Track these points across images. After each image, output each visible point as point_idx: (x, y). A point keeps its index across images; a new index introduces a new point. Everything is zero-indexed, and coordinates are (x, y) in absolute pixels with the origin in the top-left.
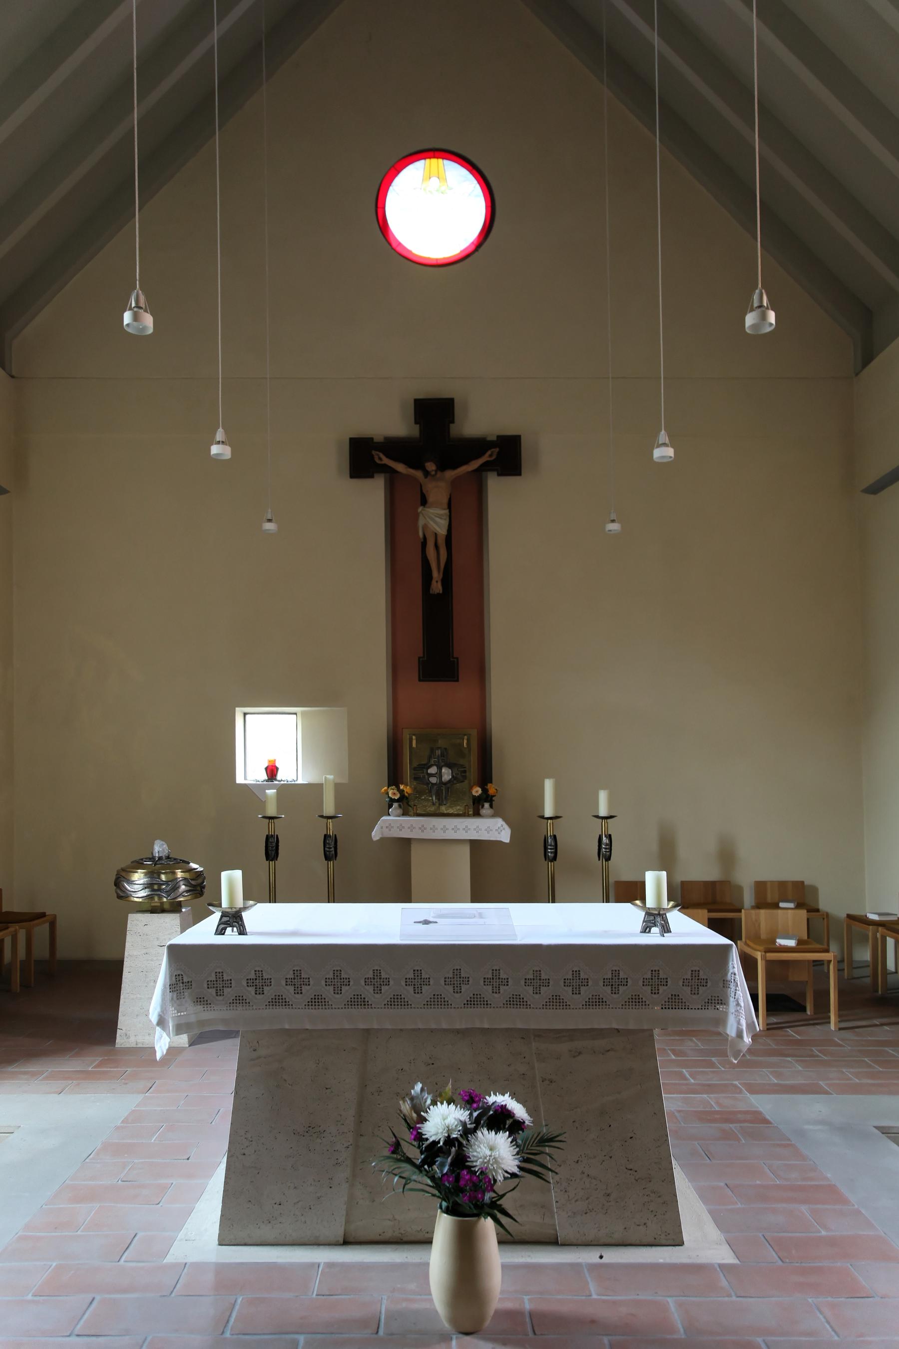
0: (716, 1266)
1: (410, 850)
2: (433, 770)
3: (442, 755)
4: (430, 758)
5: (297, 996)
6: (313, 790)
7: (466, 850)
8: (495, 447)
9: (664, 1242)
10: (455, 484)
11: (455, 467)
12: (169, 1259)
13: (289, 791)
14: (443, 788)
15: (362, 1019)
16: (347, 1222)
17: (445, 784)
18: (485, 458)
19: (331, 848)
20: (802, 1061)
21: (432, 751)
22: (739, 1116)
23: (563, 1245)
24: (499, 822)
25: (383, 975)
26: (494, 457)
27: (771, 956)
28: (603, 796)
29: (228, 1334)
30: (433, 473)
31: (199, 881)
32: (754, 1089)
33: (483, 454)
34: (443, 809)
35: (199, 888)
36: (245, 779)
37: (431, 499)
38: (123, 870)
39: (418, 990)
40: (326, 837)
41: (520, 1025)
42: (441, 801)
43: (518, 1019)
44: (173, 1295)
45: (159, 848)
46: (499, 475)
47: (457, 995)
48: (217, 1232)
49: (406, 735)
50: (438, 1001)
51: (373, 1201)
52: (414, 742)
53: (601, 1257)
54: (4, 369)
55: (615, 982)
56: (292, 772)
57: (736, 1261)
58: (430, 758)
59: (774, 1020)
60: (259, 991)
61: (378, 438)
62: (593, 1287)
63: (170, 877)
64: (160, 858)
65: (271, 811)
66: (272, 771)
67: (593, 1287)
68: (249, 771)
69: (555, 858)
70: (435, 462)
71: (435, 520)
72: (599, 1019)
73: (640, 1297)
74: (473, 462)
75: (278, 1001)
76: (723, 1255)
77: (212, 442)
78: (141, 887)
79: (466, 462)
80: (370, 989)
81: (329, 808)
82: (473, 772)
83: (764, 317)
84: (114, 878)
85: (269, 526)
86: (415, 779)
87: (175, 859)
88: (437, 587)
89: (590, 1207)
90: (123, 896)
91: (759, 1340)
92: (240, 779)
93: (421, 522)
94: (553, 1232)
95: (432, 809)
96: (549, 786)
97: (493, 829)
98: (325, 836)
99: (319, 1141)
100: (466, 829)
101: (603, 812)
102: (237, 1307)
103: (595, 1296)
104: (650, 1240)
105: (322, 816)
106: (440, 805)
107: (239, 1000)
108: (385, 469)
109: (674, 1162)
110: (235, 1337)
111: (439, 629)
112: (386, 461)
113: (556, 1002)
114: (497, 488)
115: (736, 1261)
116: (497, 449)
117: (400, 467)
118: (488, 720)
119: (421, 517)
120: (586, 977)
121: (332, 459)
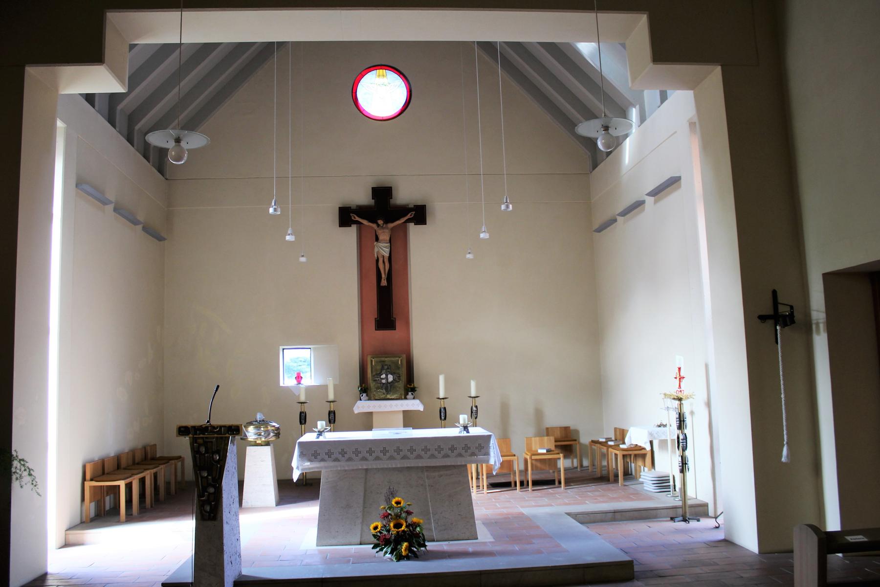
2: (383, 376)
6: (323, 388)
7: (401, 416)
11: (393, 222)
13: (309, 390)
15: (365, 465)
18: (408, 216)
21: (383, 367)
24: (417, 402)
27: (534, 457)
28: (473, 384)
32: (522, 507)
34: (389, 396)
37: (381, 238)
39: (385, 455)
40: (330, 413)
43: (421, 463)
45: (259, 417)
49: (369, 359)
54: (163, 175)
55: (370, 452)
56: (310, 380)
61: (354, 207)
65: (303, 399)
66: (299, 378)
68: (287, 381)
69: (445, 419)
70: (383, 214)
71: (383, 249)
75: (336, 460)
77: (286, 234)
79: (398, 219)
81: (331, 397)
82: (404, 378)
83: (507, 207)
85: (303, 259)
88: (384, 283)
92: (281, 384)
93: (376, 250)
96: (442, 378)
97: (414, 405)
100: (402, 405)
101: (473, 394)
107: (323, 460)
111: (385, 304)
112: (357, 219)
114: (413, 230)
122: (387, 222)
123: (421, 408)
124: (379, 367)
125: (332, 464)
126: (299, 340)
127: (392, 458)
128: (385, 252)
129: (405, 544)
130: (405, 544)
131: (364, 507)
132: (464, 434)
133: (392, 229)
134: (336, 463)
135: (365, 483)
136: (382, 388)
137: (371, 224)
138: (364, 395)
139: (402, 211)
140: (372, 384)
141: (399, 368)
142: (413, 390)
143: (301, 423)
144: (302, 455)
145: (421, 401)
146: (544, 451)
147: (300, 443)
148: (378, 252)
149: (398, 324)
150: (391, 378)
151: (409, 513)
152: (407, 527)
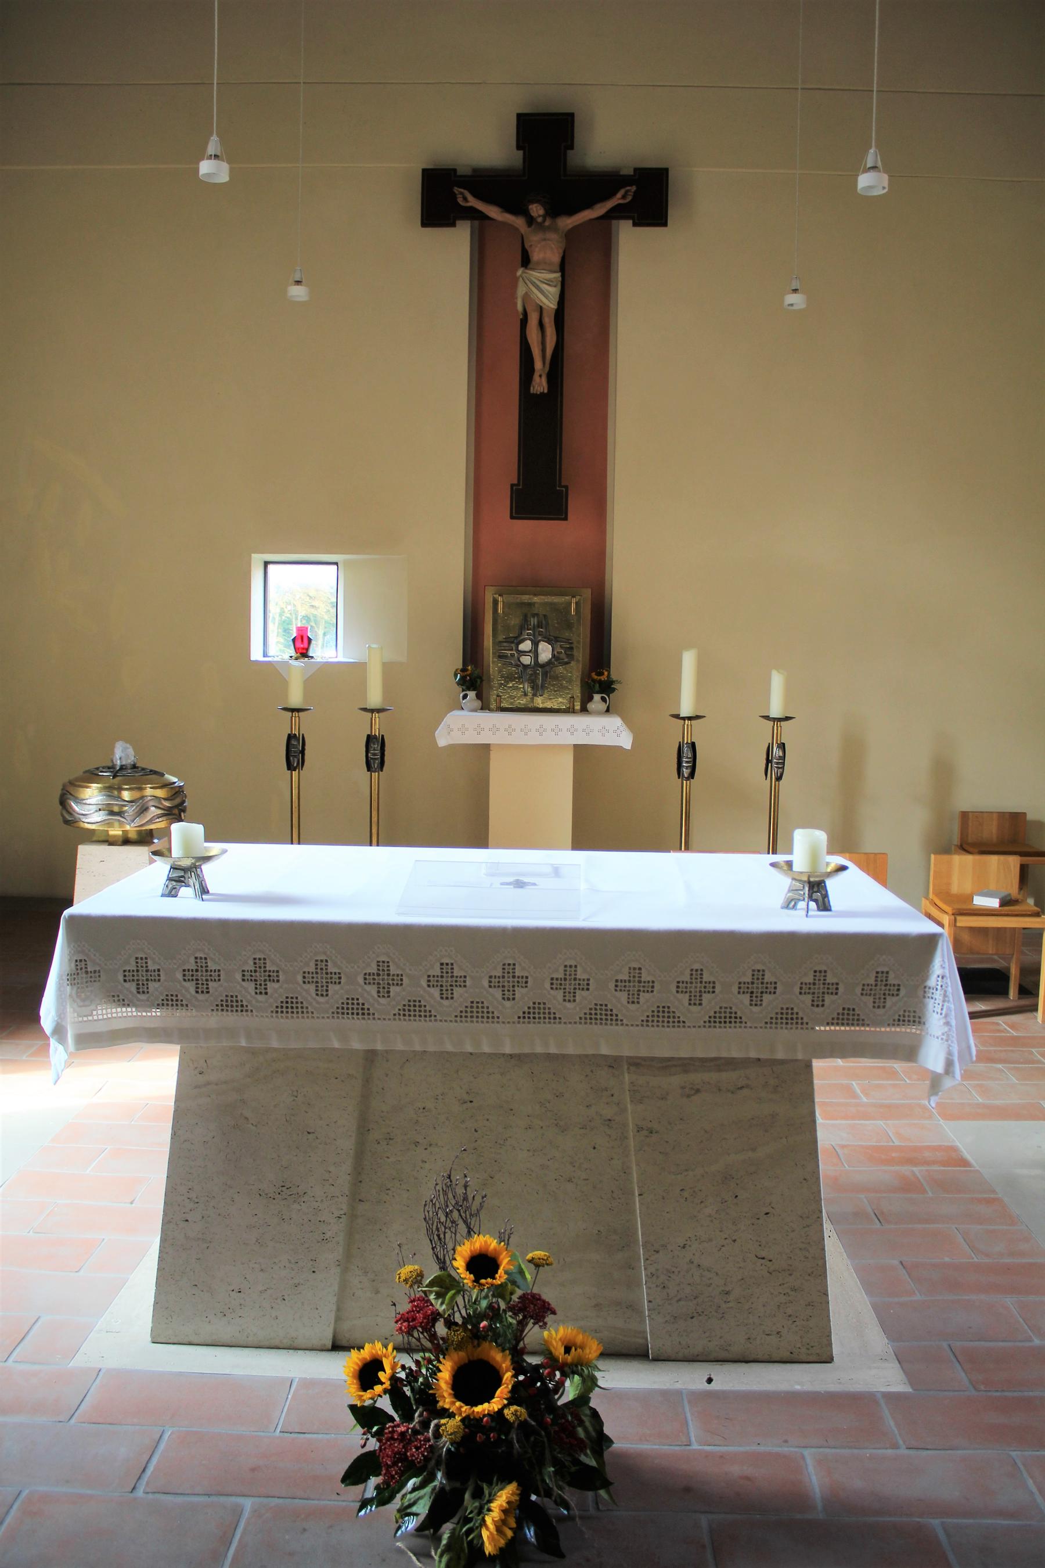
0: (879, 1396)
1: (488, 759)
2: (526, 646)
3: (540, 625)
4: (522, 628)
5: (259, 997)
7: (569, 759)
8: (631, 185)
9: (804, 1358)
10: (571, 237)
11: (571, 212)
12: (79, 1361)
14: (540, 671)
15: (357, 1037)
16: (338, 1319)
17: (542, 666)
18: (616, 200)
19: (376, 753)
20: (1017, 1069)
22: (927, 1154)
23: (656, 1359)
24: (614, 722)
25: (393, 970)
26: (629, 198)
28: (777, 682)
29: (140, 1493)
30: (540, 220)
31: (177, 801)
33: (613, 194)
34: (539, 702)
35: (176, 811)
36: (265, 655)
37: (536, 256)
38: (71, 783)
40: (370, 739)
41: (604, 1050)
42: (537, 689)
44: (73, 1421)
45: (122, 753)
46: (635, 225)
47: (508, 1004)
48: (150, 1325)
50: (477, 1011)
51: (377, 1292)
52: (500, 606)
53: (710, 1381)
57: (908, 1389)
58: (522, 628)
59: (981, 1006)
60: (202, 989)
62: (694, 1430)
63: (137, 794)
64: (122, 768)
65: (295, 699)
66: (302, 645)
67: (694, 1430)
68: (267, 644)
69: (692, 775)
71: (541, 288)
72: (728, 1043)
73: (762, 1449)
74: (599, 205)
75: (231, 1004)
76: (887, 1378)
78: (94, 808)
79: (589, 205)
80: (373, 990)
81: (375, 697)
84: (60, 792)
85: (298, 293)
86: (500, 657)
87: (143, 769)
89: (700, 1310)
90: (70, 821)
91: (936, 1522)
93: (521, 290)
94: (641, 1341)
95: (523, 702)
96: (689, 660)
98: (369, 737)
99: (296, 1206)
101: (775, 712)
102: (162, 1446)
103: (695, 1446)
104: (786, 1355)
105: (365, 710)
106: (535, 695)
107: (171, 1001)
108: (472, 214)
109: (827, 1226)
110: (150, 1496)
111: (542, 449)
112: (473, 202)
113: (664, 1016)
114: (632, 242)
115: (908, 1389)
116: (634, 188)
117: (493, 212)
118: (607, 577)
119: (521, 283)
120: (712, 979)
121: (409, 198)
122: (555, 211)
123: (625, 740)
124: (515, 621)
125: (213, 1020)
126: (306, 541)
127: (477, 1011)
128: (547, 296)
129: (504, 1496)
130: (504, 1496)
131: (356, 1198)
132: (806, 921)
133: (571, 237)
134: (230, 1019)
135: (365, 1098)
136: (520, 678)
137: (509, 218)
138: (472, 694)
139: (602, 184)
140: (493, 666)
141: (569, 626)
142: (607, 688)
143: (290, 767)
144: (83, 973)
145: (623, 719)
146: (994, 903)
147: (72, 918)
148: (526, 296)
149: (574, 505)
150: (545, 652)
151: (536, 1309)
152: (514, 1398)
